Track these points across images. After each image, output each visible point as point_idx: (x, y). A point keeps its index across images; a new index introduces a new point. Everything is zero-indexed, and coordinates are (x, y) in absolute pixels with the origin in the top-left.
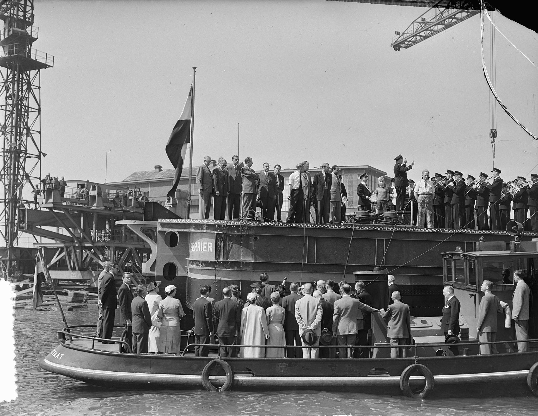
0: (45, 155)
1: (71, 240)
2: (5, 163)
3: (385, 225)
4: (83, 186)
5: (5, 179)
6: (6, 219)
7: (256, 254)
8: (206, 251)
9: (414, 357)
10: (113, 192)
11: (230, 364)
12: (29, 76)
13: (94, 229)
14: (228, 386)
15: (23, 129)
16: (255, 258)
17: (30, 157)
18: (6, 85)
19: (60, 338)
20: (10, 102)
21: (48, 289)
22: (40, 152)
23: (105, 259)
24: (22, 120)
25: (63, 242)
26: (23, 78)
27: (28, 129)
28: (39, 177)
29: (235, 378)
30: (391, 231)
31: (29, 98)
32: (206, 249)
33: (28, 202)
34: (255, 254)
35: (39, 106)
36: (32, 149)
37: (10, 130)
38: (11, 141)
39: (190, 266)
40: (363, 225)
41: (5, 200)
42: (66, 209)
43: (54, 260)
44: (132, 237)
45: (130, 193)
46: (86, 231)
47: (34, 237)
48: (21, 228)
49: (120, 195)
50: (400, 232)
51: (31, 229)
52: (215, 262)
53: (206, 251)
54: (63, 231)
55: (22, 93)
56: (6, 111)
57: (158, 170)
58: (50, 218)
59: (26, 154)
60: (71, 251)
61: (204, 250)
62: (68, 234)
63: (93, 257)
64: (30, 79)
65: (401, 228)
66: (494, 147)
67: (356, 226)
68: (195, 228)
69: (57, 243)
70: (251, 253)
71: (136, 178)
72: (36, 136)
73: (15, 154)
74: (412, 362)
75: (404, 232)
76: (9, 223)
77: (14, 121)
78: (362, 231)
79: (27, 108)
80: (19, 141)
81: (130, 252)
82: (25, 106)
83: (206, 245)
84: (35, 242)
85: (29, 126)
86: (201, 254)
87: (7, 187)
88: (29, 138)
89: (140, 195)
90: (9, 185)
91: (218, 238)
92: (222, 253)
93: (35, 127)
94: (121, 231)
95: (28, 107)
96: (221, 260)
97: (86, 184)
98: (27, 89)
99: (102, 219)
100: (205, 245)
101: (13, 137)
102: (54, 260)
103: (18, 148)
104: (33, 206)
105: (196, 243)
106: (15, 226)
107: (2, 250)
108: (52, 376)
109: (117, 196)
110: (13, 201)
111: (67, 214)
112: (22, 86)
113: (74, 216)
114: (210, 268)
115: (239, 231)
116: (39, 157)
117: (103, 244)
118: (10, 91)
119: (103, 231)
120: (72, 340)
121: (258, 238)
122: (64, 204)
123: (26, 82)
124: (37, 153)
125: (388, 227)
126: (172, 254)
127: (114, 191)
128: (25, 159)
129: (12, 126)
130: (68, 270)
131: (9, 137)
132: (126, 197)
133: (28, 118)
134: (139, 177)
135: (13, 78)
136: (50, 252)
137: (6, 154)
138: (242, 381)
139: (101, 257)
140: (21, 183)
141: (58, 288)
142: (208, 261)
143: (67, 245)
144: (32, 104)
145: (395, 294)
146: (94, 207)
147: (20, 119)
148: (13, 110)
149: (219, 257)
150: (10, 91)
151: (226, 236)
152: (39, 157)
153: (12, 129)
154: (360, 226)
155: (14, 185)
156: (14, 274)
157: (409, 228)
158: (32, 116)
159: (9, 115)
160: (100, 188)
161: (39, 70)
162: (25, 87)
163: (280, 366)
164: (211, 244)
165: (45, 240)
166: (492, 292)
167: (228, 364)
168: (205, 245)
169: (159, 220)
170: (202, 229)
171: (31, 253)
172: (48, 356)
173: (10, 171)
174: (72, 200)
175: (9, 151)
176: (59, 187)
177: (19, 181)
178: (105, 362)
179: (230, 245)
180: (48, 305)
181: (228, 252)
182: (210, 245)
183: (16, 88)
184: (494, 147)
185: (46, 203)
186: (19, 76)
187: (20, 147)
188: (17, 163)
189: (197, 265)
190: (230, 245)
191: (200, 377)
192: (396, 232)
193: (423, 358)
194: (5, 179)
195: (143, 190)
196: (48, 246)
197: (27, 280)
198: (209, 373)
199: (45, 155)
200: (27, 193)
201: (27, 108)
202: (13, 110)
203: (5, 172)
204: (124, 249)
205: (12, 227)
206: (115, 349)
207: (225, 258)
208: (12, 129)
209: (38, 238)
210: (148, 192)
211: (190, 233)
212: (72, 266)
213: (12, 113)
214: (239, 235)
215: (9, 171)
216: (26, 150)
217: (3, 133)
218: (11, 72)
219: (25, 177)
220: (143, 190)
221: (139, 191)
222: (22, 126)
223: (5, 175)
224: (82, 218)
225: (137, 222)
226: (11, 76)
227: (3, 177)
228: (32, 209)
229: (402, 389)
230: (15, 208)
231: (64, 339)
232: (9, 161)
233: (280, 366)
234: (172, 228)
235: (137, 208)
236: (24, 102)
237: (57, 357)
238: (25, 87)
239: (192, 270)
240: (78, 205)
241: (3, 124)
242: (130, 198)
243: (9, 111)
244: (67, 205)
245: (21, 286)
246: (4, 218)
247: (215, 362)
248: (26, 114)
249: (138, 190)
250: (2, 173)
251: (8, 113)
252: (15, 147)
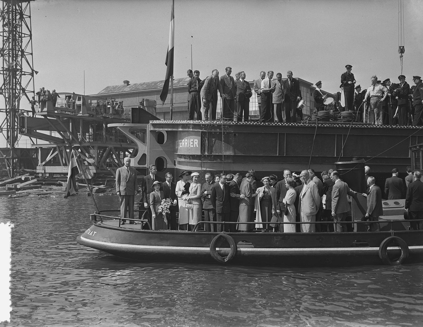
0: (37, 73)
1: (62, 141)
2: (4, 80)
3: (342, 122)
4: (70, 97)
5: (5, 93)
6: (7, 126)
7: (235, 148)
8: (192, 146)
9: (391, 231)
10: (94, 102)
11: (233, 238)
12: (21, 7)
13: (81, 132)
14: (233, 256)
15: (18, 51)
16: (235, 152)
17: (25, 75)
18: (3, 15)
19: (92, 219)
20: (7, 29)
21: (45, 181)
22: (33, 70)
23: (91, 157)
24: (17, 44)
25: (55, 143)
26: (16, 9)
27: (23, 52)
28: (33, 90)
29: (238, 249)
30: (348, 128)
31: (22, 25)
32: (193, 145)
33: (28, 112)
34: (234, 149)
35: (30, 32)
36: (26, 68)
37: (8, 52)
38: (9, 62)
39: (178, 159)
40: (324, 123)
41: (6, 109)
42: (57, 116)
43: (48, 159)
44: (111, 138)
45: (108, 103)
46: (74, 133)
47: (31, 139)
48: (22, 133)
49: (100, 104)
50: (355, 128)
51: (31, 133)
52: (201, 155)
53: (192, 146)
54: (56, 134)
55: (16, 22)
56: (4, 36)
57: (126, 84)
58: (45, 124)
59: (21, 71)
60: (62, 150)
61: (191, 146)
62: (60, 137)
63: (81, 155)
64: (22, 9)
65: (356, 125)
66: (402, 60)
67: (319, 124)
69: (51, 144)
70: (231, 148)
71: (109, 91)
72: (29, 57)
73: (12, 72)
74: (390, 234)
75: (359, 128)
76: (11, 128)
77: (10, 44)
78: (324, 127)
79: (20, 34)
80: (15, 61)
81: (111, 150)
82: (19, 33)
83: (193, 142)
84: (32, 143)
85: (23, 48)
86: (189, 149)
87: (7, 99)
88: (23, 59)
89: (117, 104)
90: (9, 98)
91: (203, 135)
92: (206, 148)
93: (28, 50)
94: (103, 134)
95: (22, 33)
97: (72, 95)
98: (20, 18)
99: (86, 124)
100: (192, 142)
101: (10, 58)
102: (48, 159)
103: (14, 67)
104: (31, 114)
105: (183, 140)
106: (15, 131)
107: (5, 151)
109: (98, 105)
110: (13, 111)
111: (58, 120)
112: (16, 16)
113: (64, 122)
114: (197, 161)
115: (221, 129)
116: (32, 75)
117: (89, 144)
118: (6, 21)
119: (87, 134)
120: (102, 222)
121: (237, 135)
122: (56, 112)
123: (18, 12)
124: (30, 71)
125: (345, 124)
126: (162, 149)
127: (95, 101)
128: (21, 76)
129: (9, 49)
130: (61, 165)
131: (7, 58)
132: (105, 106)
133: (22, 42)
134: (111, 91)
135: (8, 9)
136: (45, 152)
137: (5, 72)
138: (244, 251)
139: (87, 155)
140: (19, 96)
141: (52, 180)
142: (194, 155)
143: (59, 145)
144: (25, 30)
145: (370, 179)
146: (80, 114)
147: (15, 43)
148: (9, 36)
149: (204, 151)
150: (6, 21)
151: (210, 133)
152: (32, 75)
153: (9, 52)
154: (322, 124)
155: (13, 99)
156: (16, 169)
157: (363, 125)
158: (25, 40)
159: (6, 40)
160: (85, 98)
161: (29, 2)
162: (18, 17)
163: (275, 239)
164: (197, 140)
165: (41, 142)
167: (232, 238)
168: (192, 142)
169: (151, 122)
170: (189, 128)
171: (29, 153)
172: (84, 233)
173: (9, 87)
174: (61, 109)
175: (8, 70)
176: (53, 97)
177: (17, 95)
178: (130, 237)
179: (214, 142)
180: (47, 194)
181: (212, 147)
182: (196, 142)
183: (11, 17)
184: (402, 60)
185: (41, 112)
186: (13, 8)
187: (16, 66)
188: (14, 80)
189: (185, 158)
190: (214, 142)
191: (208, 249)
192: (352, 128)
193: (399, 231)
194: (5, 93)
195: (119, 100)
196: (44, 147)
197: (27, 174)
198: (215, 246)
199: (37, 73)
200: (24, 105)
201: (20, 34)
202: (9, 36)
203: (5, 87)
204: (105, 149)
205: (13, 132)
206: (138, 227)
207: (210, 152)
208: (9, 52)
209: (34, 139)
210: (123, 102)
211: (177, 132)
212: (64, 162)
213: (8, 38)
214: (220, 133)
215: (8, 86)
216: (22, 69)
217: (2, 55)
218: (6, 4)
219: (21, 91)
220: (119, 100)
221: (115, 101)
222: (17, 49)
223: (5, 89)
224: (71, 124)
225: (126, 125)
226: (6, 8)
227: (4, 91)
228: (30, 116)
229: (381, 257)
230: (14, 116)
231: (96, 220)
232: (8, 78)
233: (275, 239)
234: (162, 128)
235: (114, 114)
236: (18, 29)
237: (91, 234)
238: (18, 17)
239: (180, 163)
240: (67, 113)
241: (1, 47)
242: (109, 106)
243: (5, 37)
244: (58, 113)
245: (23, 179)
246: (6, 124)
247: (221, 236)
248: (20, 39)
249: (114, 100)
250: (3, 88)
251: (5, 38)
252: (13, 66)
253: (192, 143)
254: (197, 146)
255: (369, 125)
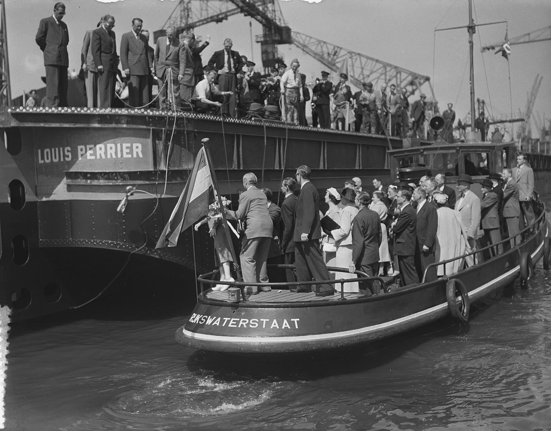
8: (130, 156)
32: (131, 152)
61: (125, 156)
68: (99, 122)
83: (131, 148)
86: (116, 162)
96: (241, 169)
100: (127, 148)
108: (496, 399)
142: (135, 173)
164: (140, 146)
166: (492, 183)
168: (127, 148)
253: (128, 151)
254: (141, 156)
255: (288, 124)
